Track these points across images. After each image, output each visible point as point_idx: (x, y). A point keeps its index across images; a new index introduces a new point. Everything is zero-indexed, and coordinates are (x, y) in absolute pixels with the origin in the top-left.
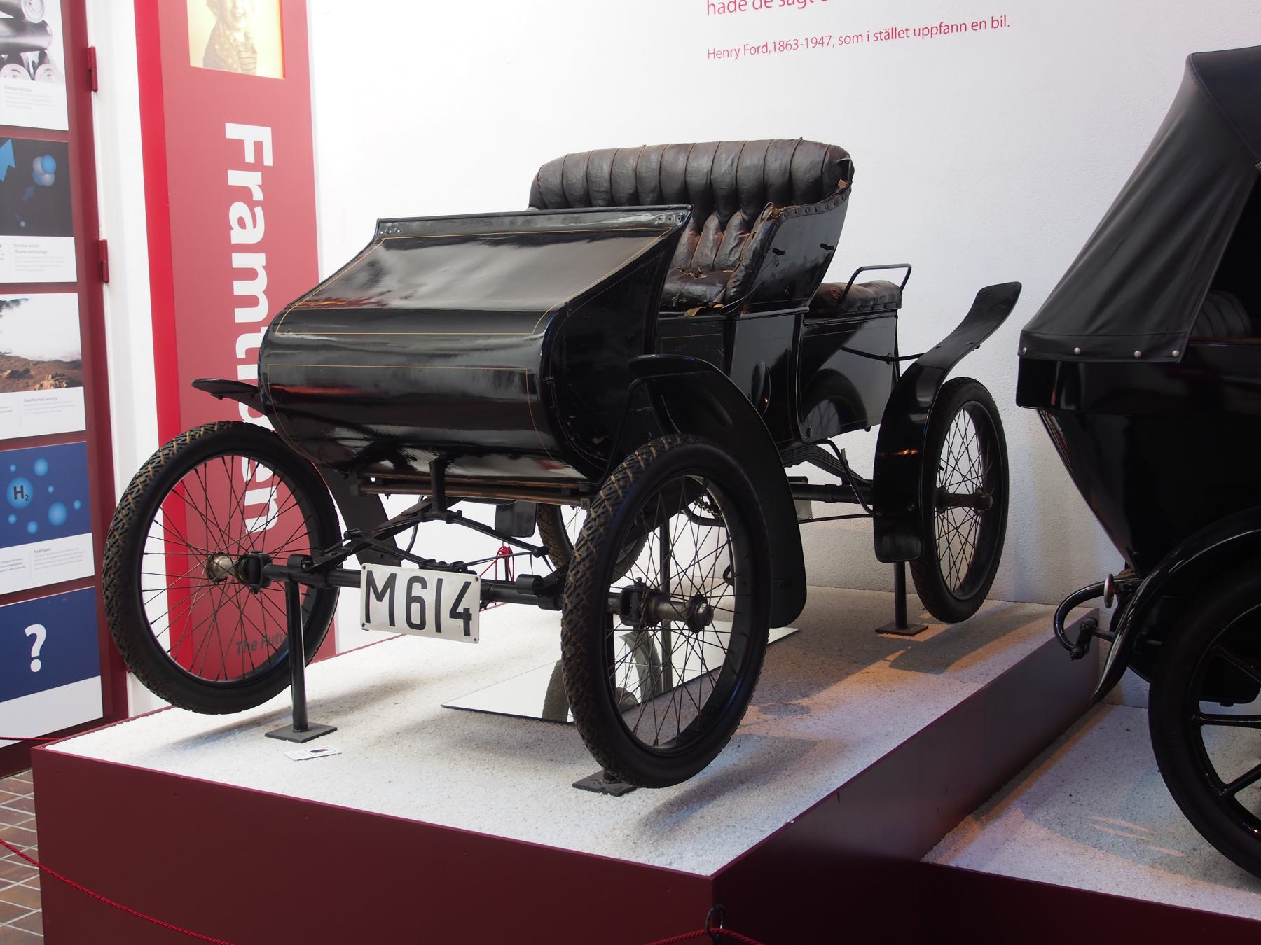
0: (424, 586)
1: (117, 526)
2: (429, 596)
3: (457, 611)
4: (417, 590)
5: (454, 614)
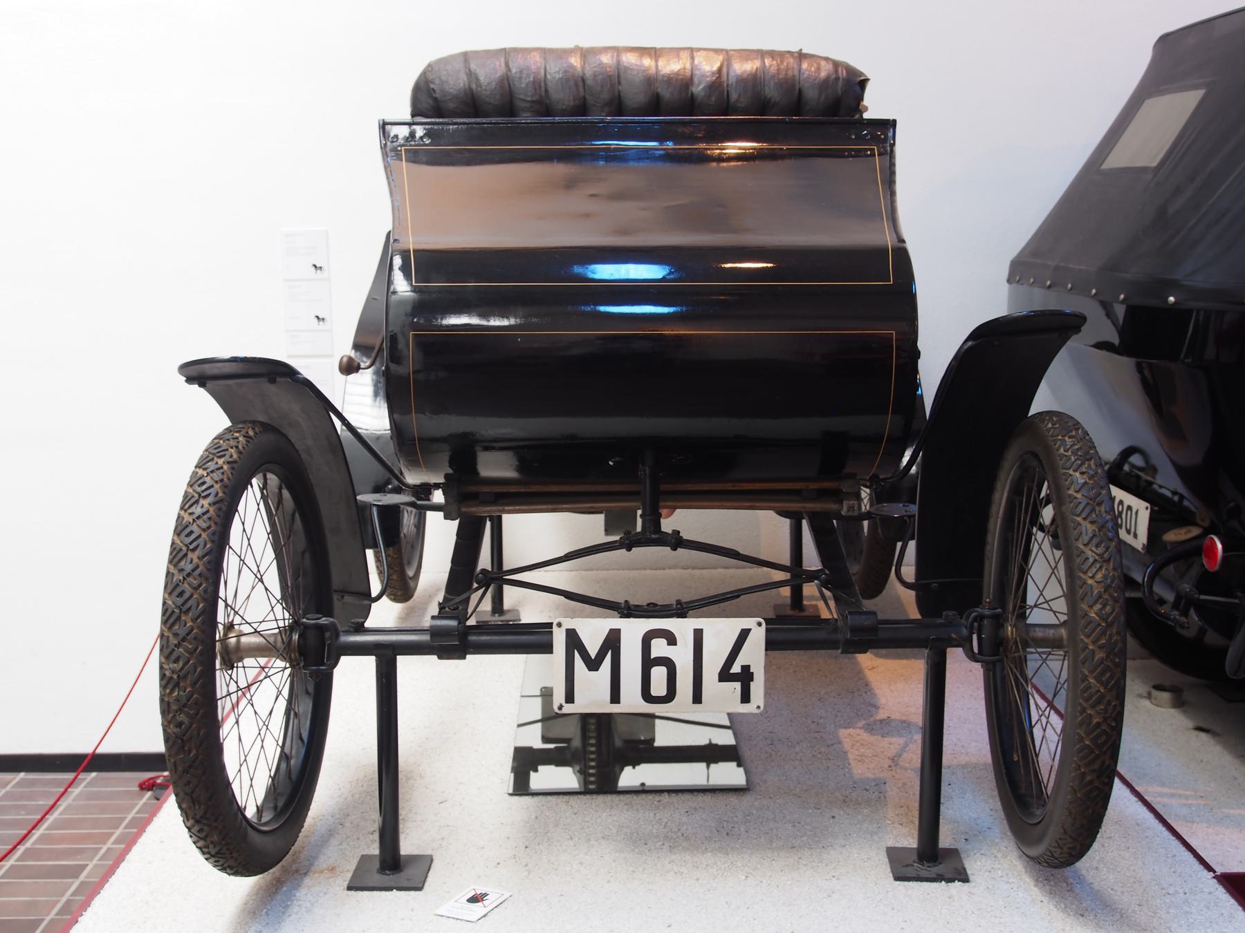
0: (671, 640)
1: (187, 606)
2: (682, 656)
3: (732, 671)
4: (659, 648)
5: (725, 675)
